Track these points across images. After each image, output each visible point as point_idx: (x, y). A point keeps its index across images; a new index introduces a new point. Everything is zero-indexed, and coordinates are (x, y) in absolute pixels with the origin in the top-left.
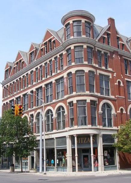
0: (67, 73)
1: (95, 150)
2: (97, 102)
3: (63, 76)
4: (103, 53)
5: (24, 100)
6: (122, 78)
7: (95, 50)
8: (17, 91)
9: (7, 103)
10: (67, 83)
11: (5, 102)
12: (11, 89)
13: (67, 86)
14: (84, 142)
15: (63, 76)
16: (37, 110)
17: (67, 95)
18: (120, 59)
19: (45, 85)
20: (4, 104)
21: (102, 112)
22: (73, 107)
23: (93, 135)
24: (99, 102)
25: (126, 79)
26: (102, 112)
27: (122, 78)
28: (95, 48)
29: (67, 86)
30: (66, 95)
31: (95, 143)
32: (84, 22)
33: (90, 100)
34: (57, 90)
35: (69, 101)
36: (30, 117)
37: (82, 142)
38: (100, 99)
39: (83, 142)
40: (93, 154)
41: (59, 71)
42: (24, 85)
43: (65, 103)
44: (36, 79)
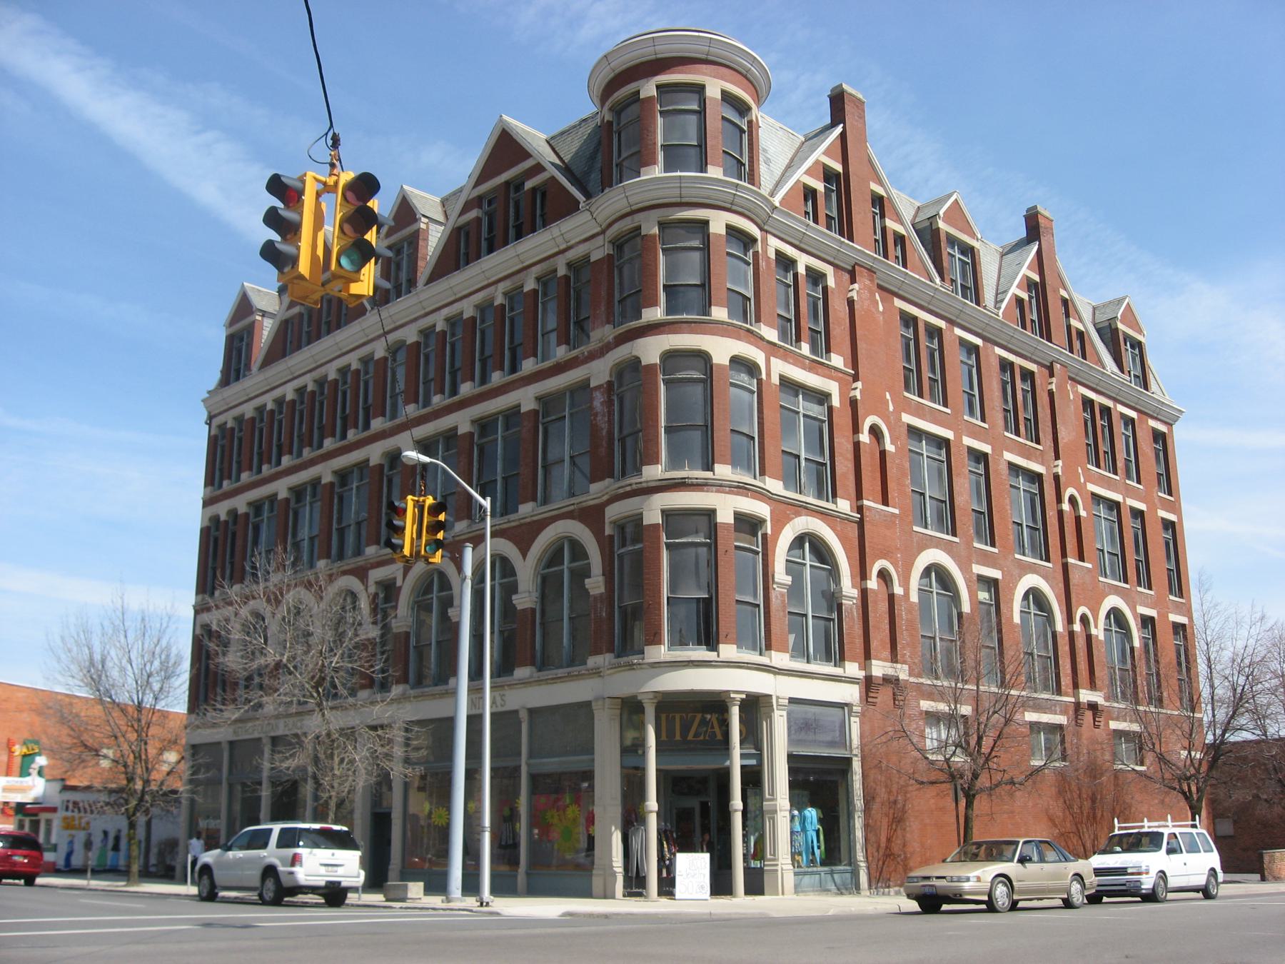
0: (611, 364)
1: (753, 779)
2: (769, 524)
3: (588, 379)
4: (801, 270)
5: (341, 499)
6: (891, 408)
7: (765, 251)
8: (239, 472)
9: (233, 513)
10: (610, 413)
11: (222, 509)
12: (223, 452)
13: (610, 433)
14: (690, 737)
15: (588, 379)
16: (798, 514)
17: (608, 481)
18: (881, 308)
19: (290, 489)
20: (215, 520)
21: (790, 578)
22: (638, 546)
23: (742, 700)
24: (779, 523)
25: (907, 418)
26: (790, 578)
27: (891, 408)
28: (765, 241)
29: (610, 433)
30: (602, 479)
31: (752, 734)
32: (719, 97)
33: (734, 511)
34: (480, 470)
35: (614, 512)
36: (376, 595)
37: (678, 737)
38: (785, 510)
39: (684, 734)
40: (1222, 874)
41: (561, 353)
42: (221, 470)
43: (597, 529)
44: (316, 431)
